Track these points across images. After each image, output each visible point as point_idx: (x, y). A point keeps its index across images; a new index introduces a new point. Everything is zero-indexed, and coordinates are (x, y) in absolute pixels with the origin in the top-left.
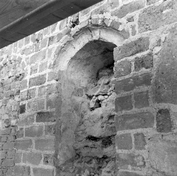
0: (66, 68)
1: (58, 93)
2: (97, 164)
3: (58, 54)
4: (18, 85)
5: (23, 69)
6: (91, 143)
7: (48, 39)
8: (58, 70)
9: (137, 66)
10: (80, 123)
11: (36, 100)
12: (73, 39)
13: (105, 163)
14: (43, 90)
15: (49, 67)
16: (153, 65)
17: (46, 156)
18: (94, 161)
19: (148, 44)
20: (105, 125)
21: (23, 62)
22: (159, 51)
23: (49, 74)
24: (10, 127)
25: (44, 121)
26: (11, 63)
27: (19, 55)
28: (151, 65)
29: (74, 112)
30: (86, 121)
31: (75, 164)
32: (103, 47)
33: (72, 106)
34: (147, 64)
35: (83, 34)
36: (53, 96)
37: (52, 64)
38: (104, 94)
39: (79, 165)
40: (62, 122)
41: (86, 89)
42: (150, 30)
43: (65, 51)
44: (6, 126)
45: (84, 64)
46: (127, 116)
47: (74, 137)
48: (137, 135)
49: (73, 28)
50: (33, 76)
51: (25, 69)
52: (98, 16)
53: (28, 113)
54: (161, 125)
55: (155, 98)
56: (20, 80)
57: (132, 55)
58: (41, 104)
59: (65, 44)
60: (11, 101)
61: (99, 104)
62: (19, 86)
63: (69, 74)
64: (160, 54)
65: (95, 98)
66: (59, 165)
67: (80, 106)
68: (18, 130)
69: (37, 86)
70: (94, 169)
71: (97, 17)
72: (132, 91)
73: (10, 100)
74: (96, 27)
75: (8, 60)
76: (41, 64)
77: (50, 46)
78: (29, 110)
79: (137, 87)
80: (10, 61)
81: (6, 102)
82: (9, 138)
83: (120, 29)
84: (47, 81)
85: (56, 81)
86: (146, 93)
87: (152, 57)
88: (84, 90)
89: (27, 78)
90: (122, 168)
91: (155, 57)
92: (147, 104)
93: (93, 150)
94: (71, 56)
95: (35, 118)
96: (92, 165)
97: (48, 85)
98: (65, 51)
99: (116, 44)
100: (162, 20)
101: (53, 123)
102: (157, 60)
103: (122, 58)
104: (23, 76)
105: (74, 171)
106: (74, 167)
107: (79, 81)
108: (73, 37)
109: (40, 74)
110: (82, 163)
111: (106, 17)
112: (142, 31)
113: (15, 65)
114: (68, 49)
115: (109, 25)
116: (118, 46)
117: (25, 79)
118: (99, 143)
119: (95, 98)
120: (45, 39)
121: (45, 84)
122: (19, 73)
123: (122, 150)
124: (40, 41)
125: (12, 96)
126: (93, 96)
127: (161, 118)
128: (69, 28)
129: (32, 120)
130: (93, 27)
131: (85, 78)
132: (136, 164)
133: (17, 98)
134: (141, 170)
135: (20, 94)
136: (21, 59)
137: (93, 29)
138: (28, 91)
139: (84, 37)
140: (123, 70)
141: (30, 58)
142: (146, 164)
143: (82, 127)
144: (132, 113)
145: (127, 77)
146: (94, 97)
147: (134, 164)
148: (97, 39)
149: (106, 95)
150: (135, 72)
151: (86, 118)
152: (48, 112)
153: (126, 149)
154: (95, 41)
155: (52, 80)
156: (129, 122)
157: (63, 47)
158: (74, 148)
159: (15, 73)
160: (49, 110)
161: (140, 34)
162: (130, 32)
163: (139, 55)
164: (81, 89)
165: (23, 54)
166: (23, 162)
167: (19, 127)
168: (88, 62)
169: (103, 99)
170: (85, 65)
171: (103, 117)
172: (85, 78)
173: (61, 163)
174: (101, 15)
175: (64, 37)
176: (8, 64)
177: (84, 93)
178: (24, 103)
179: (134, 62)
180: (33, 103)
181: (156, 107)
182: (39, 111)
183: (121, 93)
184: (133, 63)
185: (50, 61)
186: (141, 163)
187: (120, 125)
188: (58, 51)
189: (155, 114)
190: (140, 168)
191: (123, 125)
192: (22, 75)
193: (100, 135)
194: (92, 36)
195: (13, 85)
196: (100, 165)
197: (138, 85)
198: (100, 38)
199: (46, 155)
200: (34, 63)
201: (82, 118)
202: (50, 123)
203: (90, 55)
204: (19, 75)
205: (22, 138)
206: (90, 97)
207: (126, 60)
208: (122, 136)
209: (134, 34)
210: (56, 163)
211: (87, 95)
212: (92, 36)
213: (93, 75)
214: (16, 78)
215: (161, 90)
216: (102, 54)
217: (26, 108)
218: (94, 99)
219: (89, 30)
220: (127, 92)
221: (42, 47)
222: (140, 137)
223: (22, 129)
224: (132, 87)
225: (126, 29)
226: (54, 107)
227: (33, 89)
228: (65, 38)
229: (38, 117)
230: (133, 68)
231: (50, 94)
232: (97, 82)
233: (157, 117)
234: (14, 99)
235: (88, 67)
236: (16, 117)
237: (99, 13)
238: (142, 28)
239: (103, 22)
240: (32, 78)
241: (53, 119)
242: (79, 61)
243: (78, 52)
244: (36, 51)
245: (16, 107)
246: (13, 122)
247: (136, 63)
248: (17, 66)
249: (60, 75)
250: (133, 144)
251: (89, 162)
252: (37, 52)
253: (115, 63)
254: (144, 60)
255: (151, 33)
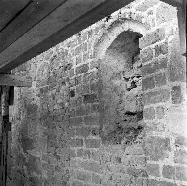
0: (104, 57)
1: (99, 78)
2: (134, 133)
3: (97, 45)
4: (67, 73)
5: (70, 60)
6: (128, 118)
7: (88, 33)
8: (97, 59)
9: (156, 53)
10: (119, 101)
11: (82, 86)
12: (108, 31)
13: (140, 132)
14: (87, 76)
15: (90, 57)
16: (168, 51)
17: (93, 129)
18: (131, 132)
19: (164, 34)
20: (139, 102)
21: (70, 54)
22: (172, 39)
23: (91, 62)
24: (65, 109)
25: (90, 102)
26: (60, 55)
27: (66, 48)
28: (167, 51)
29: (114, 93)
30: (125, 100)
31: (117, 135)
32: (135, 36)
33: (112, 89)
34: (164, 50)
35: (116, 26)
36: (95, 81)
37: (93, 54)
38: (138, 76)
39: (120, 135)
40: (104, 102)
41: (124, 73)
42: (165, 21)
43: (102, 42)
44: (61, 108)
45: (120, 51)
46: (151, 93)
47: (115, 113)
48: (158, 107)
49: (107, 22)
50: (78, 65)
51: (71, 59)
52: (126, 11)
53: (77, 96)
54: (175, 98)
55: (170, 78)
56: (69, 70)
57: (153, 43)
58: (86, 88)
59: (101, 37)
60: (63, 87)
61: (134, 84)
62: (68, 74)
63: (107, 61)
64: (173, 42)
65: (131, 80)
66: (104, 136)
67: (118, 87)
68: (71, 110)
69: (82, 74)
70: (131, 137)
71: (125, 12)
72: (153, 73)
73: (62, 87)
74: (125, 20)
75: (57, 53)
76: (83, 55)
77: (90, 38)
78: (78, 94)
79: (157, 70)
80: (59, 53)
81: (59, 88)
82: (65, 118)
83: (143, 22)
84: (89, 69)
85: (96, 69)
86: (163, 74)
87: (168, 44)
88: (121, 74)
89: (74, 67)
90: (148, 134)
91: (170, 44)
92: (165, 83)
93: (131, 123)
94: (107, 46)
95: (83, 101)
96: (130, 135)
97: (91, 72)
98: (102, 42)
99: (141, 33)
100: (174, 13)
101: (98, 103)
102: (170, 47)
103: (145, 47)
104: (71, 66)
105: (116, 139)
106: (116, 137)
107: (117, 67)
108: (108, 30)
109: (84, 63)
110: (123, 134)
111: (131, 12)
112: (159, 23)
113: (64, 57)
114: (104, 40)
115: (134, 19)
116: (144, 35)
117: (72, 68)
118: (135, 117)
119: (131, 80)
120: (85, 33)
121: (88, 72)
122: (67, 64)
123: (148, 120)
124: (81, 35)
125: (63, 83)
126: (130, 78)
127: (174, 93)
128: (104, 22)
129: (81, 102)
130: (123, 20)
131: (122, 63)
132: (158, 129)
133: (67, 85)
134: (161, 134)
135: (70, 81)
136: (68, 51)
137: (123, 22)
138: (76, 78)
139: (116, 29)
140: (146, 57)
141: (74, 50)
142: (165, 129)
143: (121, 105)
144: (154, 91)
145: (150, 62)
146: (130, 79)
147: (156, 130)
148: (127, 30)
149: (140, 76)
150: (155, 58)
151: (124, 98)
152: (92, 95)
153: (151, 119)
154: (126, 32)
155: (93, 68)
156: (152, 98)
157: (100, 39)
158: (116, 122)
159: (64, 64)
160: (93, 93)
161: (158, 25)
162: (151, 24)
163: (158, 43)
164: (119, 73)
165: (68, 46)
166: (77, 136)
167: (71, 108)
168: (123, 49)
169: (137, 80)
170: (121, 52)
171: (137, 96)
172: (122, 63)
173: (105, 134)
174: (128, 9)
175: (100, 31)
176: (57, 56)
177: (122, 76)
178: (73, 89)
179: (154, 49)
180: (81, 88)
181: (171, 85)
182: (85, 94)
183: (146, 75)
184: (154, 50)
185: (91, 51)
186: (162, 129)
187: (146, 101)
188: (96, 43)
189: (170, 91)
190: (161, 132)
191: (148, 100)
192: (70, 65)
193: (135, 110)
194: (123, 28)
195: (63, 74)
196: (136, 135)
197: (157, 69)
198: (129, 29)
199: (94, 128)
200: (78, 54)
201: (121, 97)
202: (94, 104)
203: (123, 43)
204: (67, 66)
205: (74, 117)
206: (127, 79)
207: (149, 48)
208: (147, 109)
209: (154, 26)
210: (101, 134)
211: (124, 78)
212: (123, 28)
213: (129, 60)
214: (65, 68)
215: (174, 71)
216: (134, 41)
217: (75, 93)
218: (130, 81)
219: (120, 22)
220: (150, 75)
221: (84, 40)
222: (160, 109)
223: (73, 110)
224: (153, 70)
225: (147, 22)
226: (97, 90)
227: (80, 76)
228: (101, 31)
229: (85, 99)
230: (154, 55)
231: (93, 79)
232: (133, 65)
233: (172, 93)
234: (65, 85)
235: (123, 53)
236: (68, 101)
237: (127, 8)
238: (160, 20)
239: (130, 15)
240: (78, 67)
241: (97, 100)
242: (115, 49)
243: (113, 42)
244: (79, 44)
245: (67, 92)
246: (66, 104)
247: (156, 50)
248: (65, 58)
249: (99, 63)
250: (156, 114)
251: (128, 132)
252: (80, 45)
253: (140, 51)
254: (162, 48)
255: (166, 25)
